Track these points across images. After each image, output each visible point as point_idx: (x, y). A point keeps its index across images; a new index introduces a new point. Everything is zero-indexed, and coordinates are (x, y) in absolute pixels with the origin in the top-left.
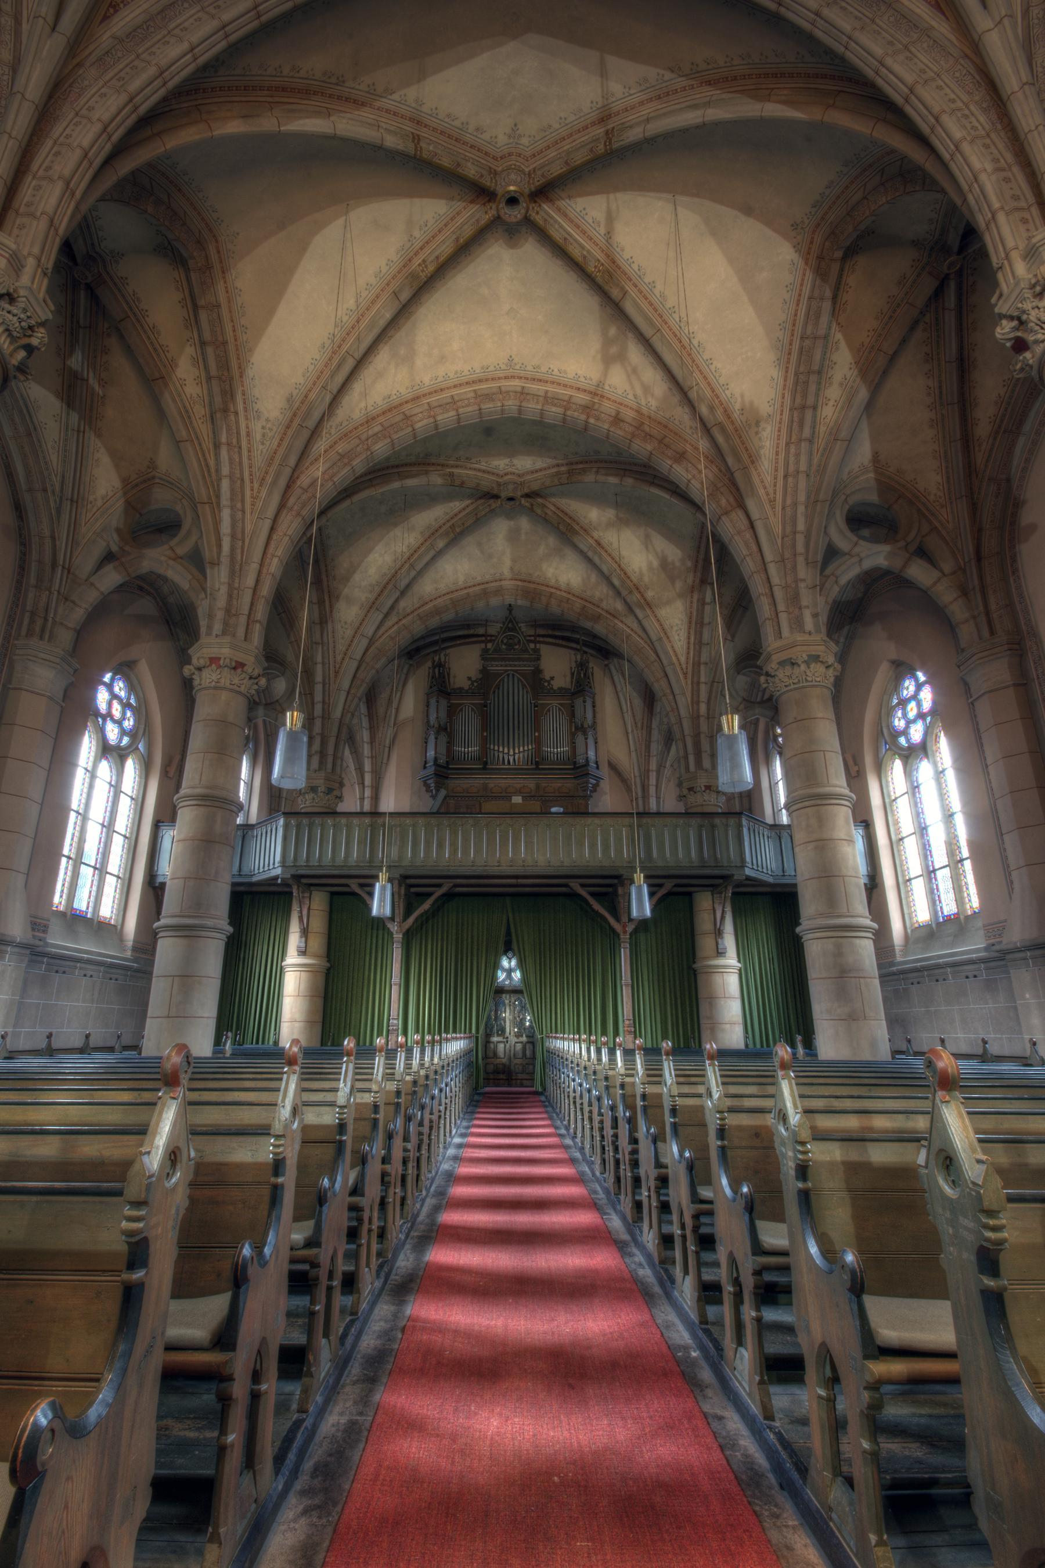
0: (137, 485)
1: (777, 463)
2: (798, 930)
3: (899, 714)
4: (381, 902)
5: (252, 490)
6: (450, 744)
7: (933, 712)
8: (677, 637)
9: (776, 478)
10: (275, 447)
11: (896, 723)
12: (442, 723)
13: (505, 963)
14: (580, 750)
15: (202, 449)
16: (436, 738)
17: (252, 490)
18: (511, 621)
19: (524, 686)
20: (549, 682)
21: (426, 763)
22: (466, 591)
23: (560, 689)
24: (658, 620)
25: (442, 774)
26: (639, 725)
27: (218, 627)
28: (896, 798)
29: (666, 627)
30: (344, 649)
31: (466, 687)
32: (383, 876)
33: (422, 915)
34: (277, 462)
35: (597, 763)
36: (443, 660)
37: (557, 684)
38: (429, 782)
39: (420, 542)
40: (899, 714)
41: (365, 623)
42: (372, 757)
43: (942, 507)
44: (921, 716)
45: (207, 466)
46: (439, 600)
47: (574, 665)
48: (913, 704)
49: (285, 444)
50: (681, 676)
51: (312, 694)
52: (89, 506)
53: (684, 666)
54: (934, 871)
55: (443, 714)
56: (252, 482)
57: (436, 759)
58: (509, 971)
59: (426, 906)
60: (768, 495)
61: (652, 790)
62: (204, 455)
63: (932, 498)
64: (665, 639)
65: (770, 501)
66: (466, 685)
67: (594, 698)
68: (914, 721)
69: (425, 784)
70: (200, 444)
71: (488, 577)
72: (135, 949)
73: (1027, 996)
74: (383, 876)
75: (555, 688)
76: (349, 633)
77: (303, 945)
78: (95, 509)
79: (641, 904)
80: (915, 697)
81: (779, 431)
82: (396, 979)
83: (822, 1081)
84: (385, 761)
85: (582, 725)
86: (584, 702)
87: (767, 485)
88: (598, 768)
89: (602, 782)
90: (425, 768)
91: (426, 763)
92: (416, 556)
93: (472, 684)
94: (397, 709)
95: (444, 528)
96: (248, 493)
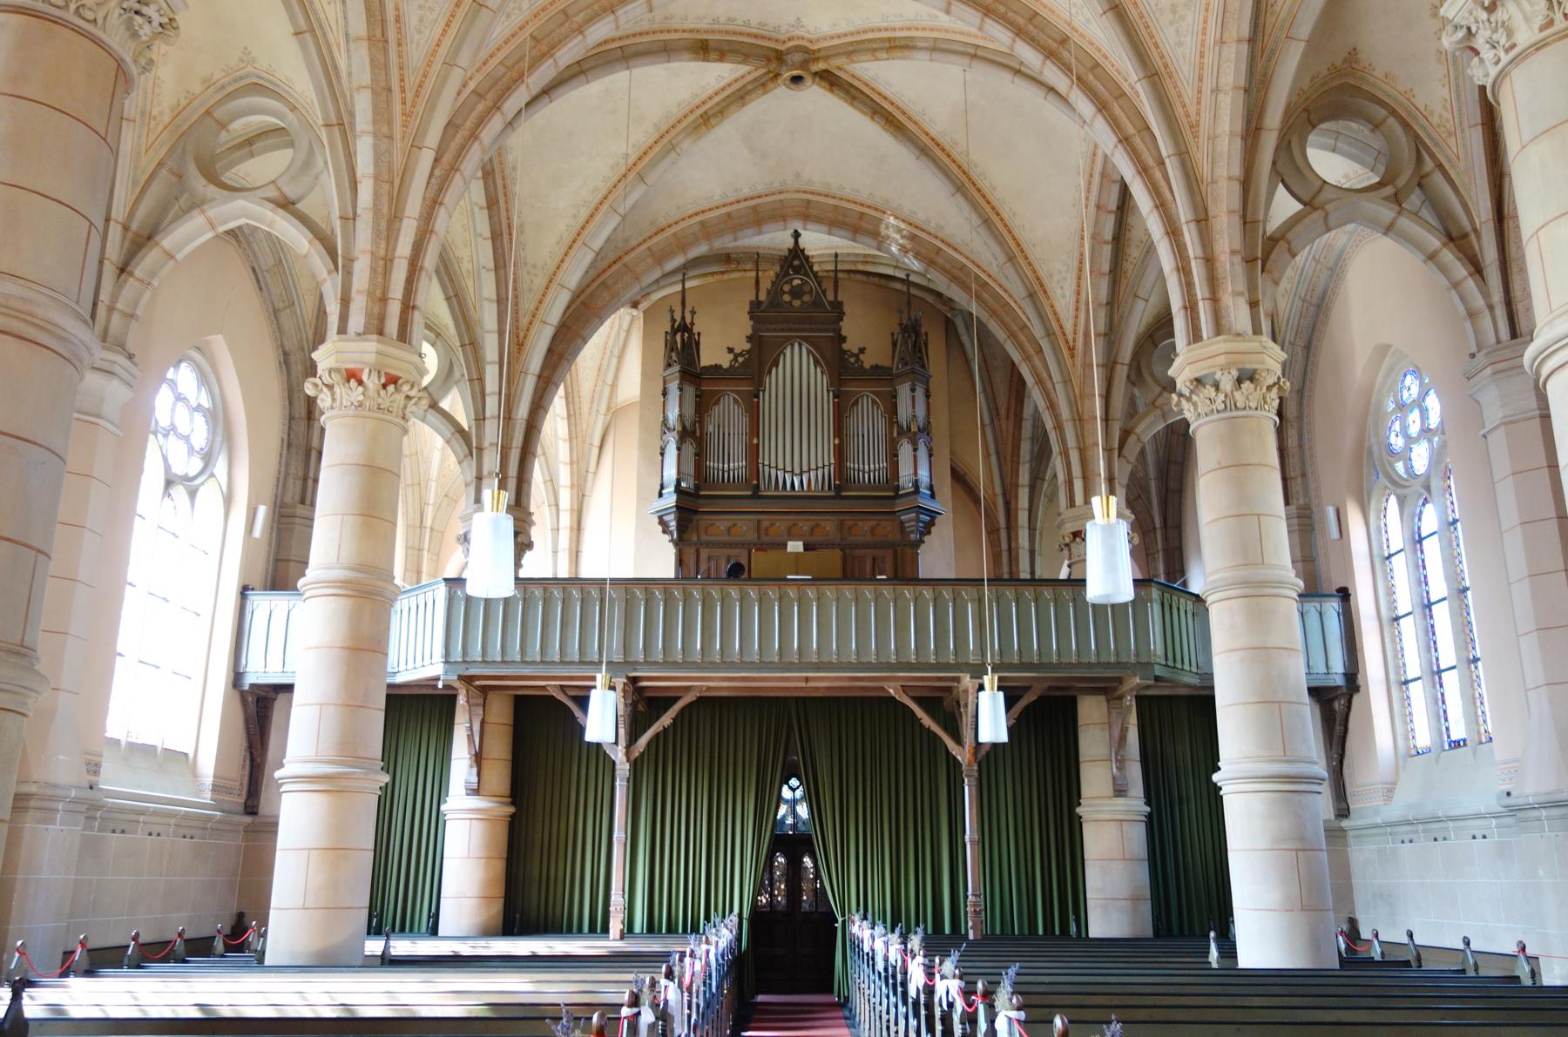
0: (222, 88)
1: (1201, 69)
2: (1215, 777)
3: (1397, 426)
4: (601, 721)
5: (404, 103)
6: (700, 457)
7: (1442, 429)
8: (1059, 292)
9: (1200, 92)
10: (437, 37)
11: (1393, 439)
12: (688, 424)
13: (786, 793)
14: (905, 472)
15: (327, 42)
16: (679, 449)
17: (404, 103)
18: (802, 265)
19: (817, 363)
20: (857, 356)
21: (662, 487)
22: (724, 210)
23: (876, 368)
24: (1030, 264)
25: (690, 515)
26: (1003, 411)
27: (357, 321)
28: (1390, 556)
29: (1042, 275)
30: (532, 308)
31: (726, 365)
32: (601, 678)
33: (657, 735)
34: (439, 59)
35: (931, 488)
36: (688, 321)
37: (868, 361)
38: (666, 518)
39: (652, 140)
40: (1397, 426)
41: (565, 265)
42: (572, 463)
43: (1450, 135)
44: (1426, 432)
45: (336, 68)
46: (682, 225)
47: (897, 329)
48: (1415, 415)
49: (453, 31)
50: (1066, 352)
51: (481, 380)
52: (153, 123)
53: (1070, 338)
54: (1440, 672)
55: (690, 411)
56: (403, 91)
57: (678, 482)
58: (793, 803)
59: (666, 720)
60: (1188, 116)
61: (1023, 517)
62: (331, 52)
63: (1435, 120)
64: (1040, 294)
65: (1191, 127)
66: (725, 361)
67: (927, 384)
68: (1417, 440)
69: (662, 522)
70: (325, 35)
71: (760, 189)
72: (216, 788)
73: (1541, 873)
74: (601, 678)
75: (867, 366)
76: (540, 281)
77: (475, 779)
78: (160, 128)
79: (991, 721)
80: (1419, 403)
81: (1205, 22)
82: (619, 834)
83: (1294, 981)
84: (592, 468)
85: (909, 429)
86: (913, 390)
87: (1187, 101)
88: (933, 496)
89: (939, 520)
90: (661, 495)
91: (662, 487)
92: (647, 159)
93: (735, 359)
94: (614, 386)
95: (692, 118)
96: (397, 108)
